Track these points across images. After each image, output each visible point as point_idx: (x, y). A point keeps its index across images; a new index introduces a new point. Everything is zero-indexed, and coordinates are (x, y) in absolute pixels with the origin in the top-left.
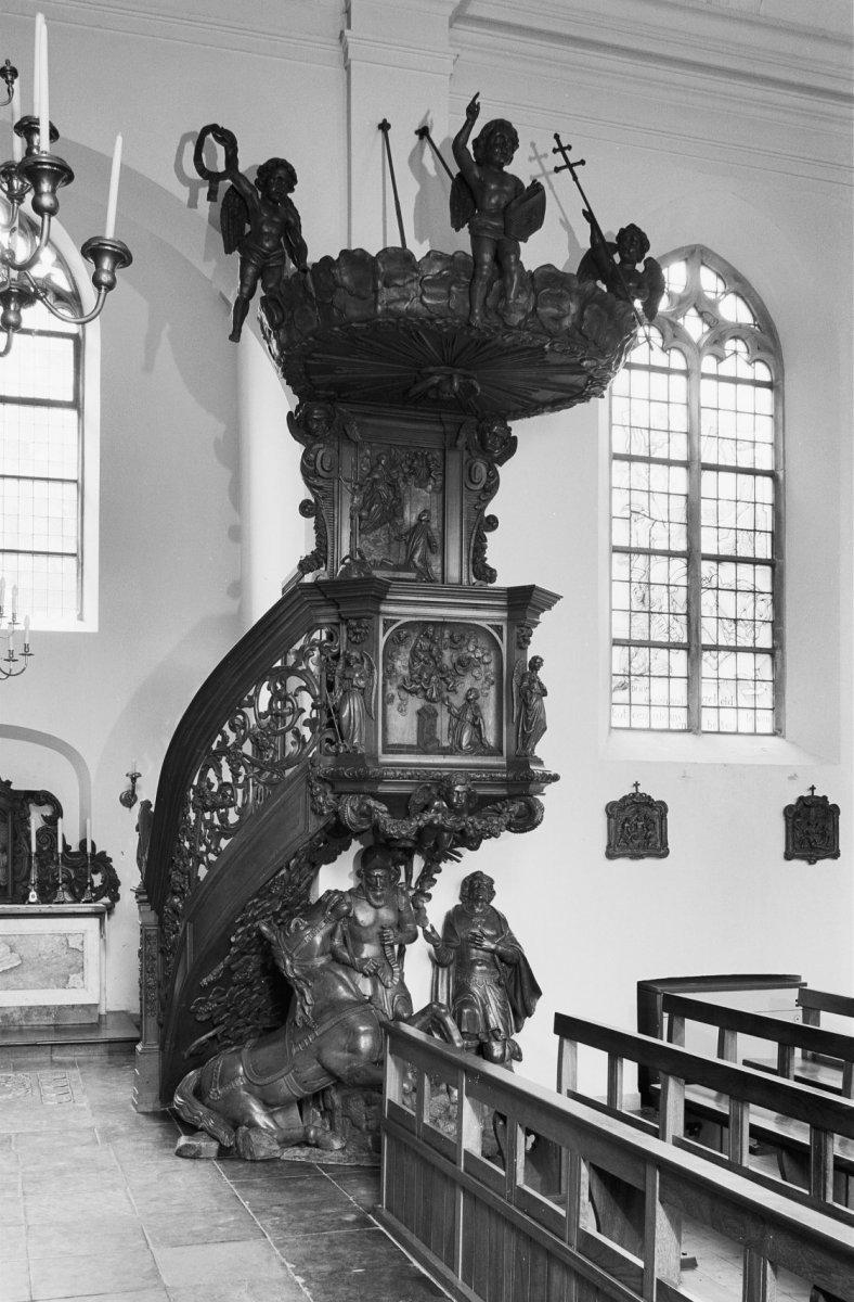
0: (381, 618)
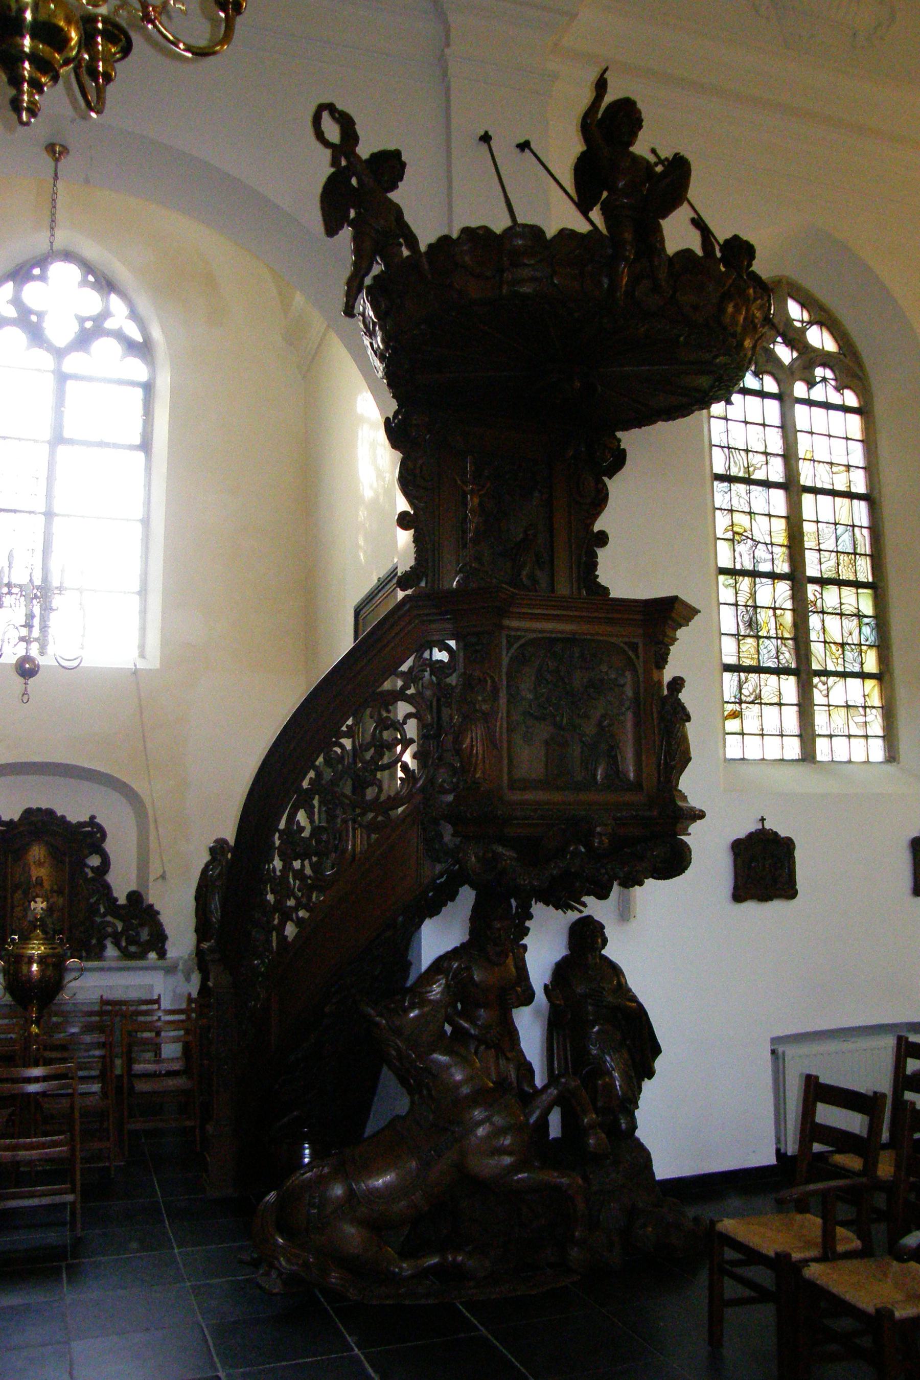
0: (504, 633)
